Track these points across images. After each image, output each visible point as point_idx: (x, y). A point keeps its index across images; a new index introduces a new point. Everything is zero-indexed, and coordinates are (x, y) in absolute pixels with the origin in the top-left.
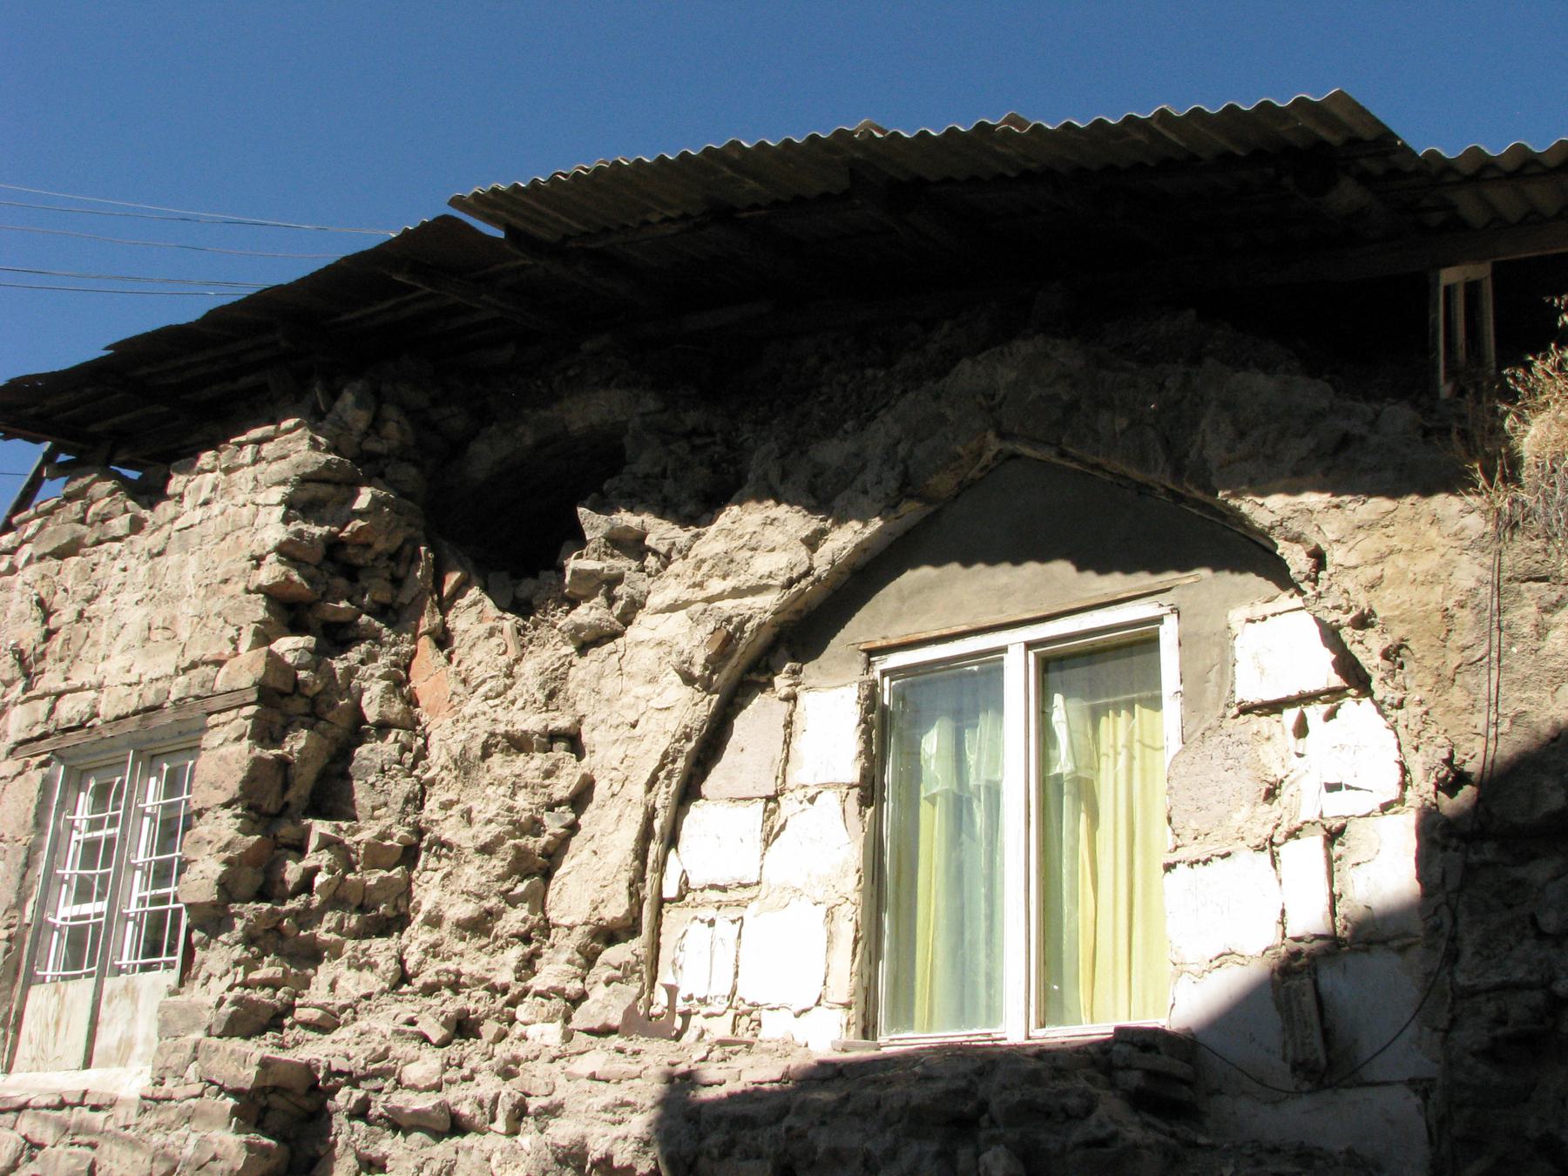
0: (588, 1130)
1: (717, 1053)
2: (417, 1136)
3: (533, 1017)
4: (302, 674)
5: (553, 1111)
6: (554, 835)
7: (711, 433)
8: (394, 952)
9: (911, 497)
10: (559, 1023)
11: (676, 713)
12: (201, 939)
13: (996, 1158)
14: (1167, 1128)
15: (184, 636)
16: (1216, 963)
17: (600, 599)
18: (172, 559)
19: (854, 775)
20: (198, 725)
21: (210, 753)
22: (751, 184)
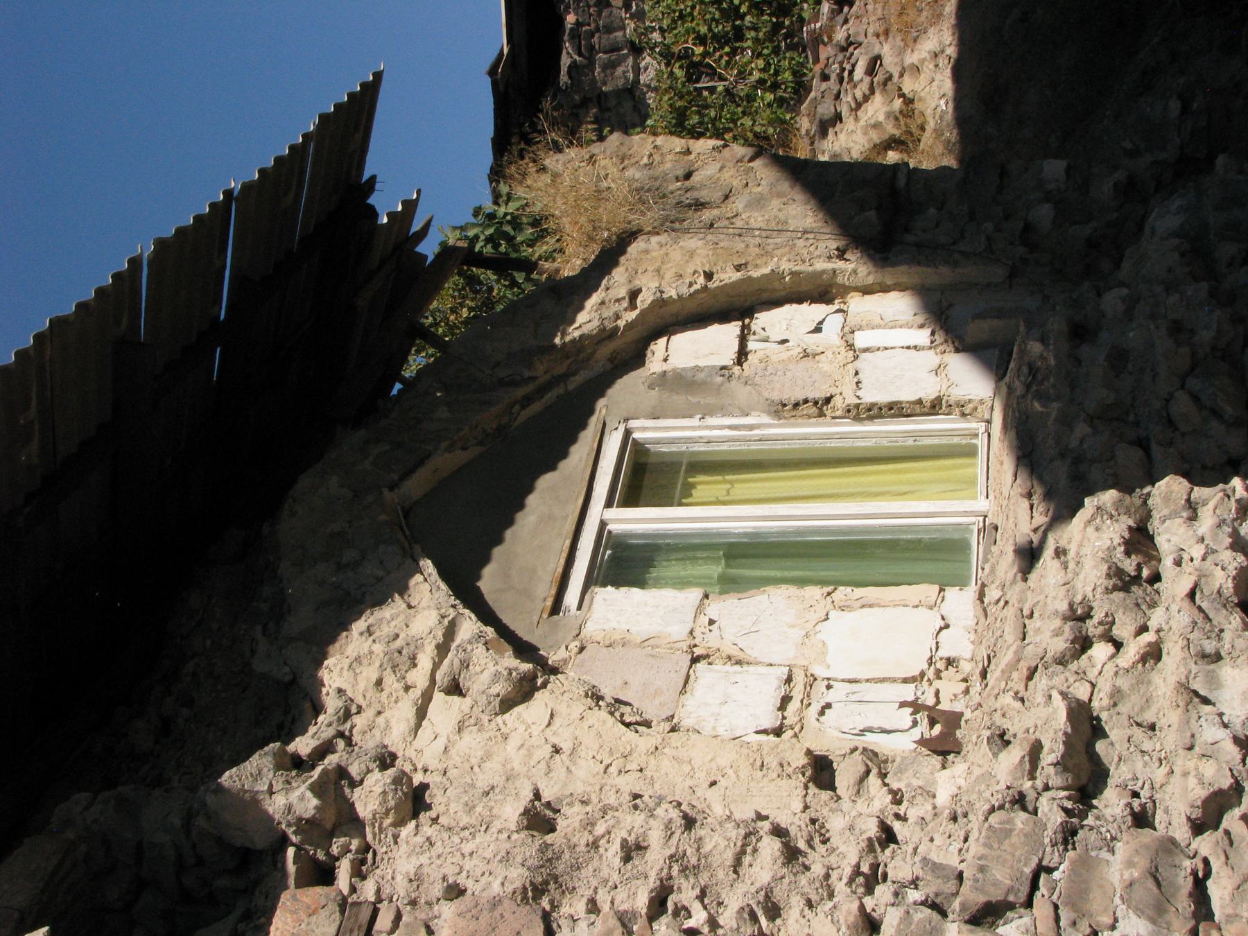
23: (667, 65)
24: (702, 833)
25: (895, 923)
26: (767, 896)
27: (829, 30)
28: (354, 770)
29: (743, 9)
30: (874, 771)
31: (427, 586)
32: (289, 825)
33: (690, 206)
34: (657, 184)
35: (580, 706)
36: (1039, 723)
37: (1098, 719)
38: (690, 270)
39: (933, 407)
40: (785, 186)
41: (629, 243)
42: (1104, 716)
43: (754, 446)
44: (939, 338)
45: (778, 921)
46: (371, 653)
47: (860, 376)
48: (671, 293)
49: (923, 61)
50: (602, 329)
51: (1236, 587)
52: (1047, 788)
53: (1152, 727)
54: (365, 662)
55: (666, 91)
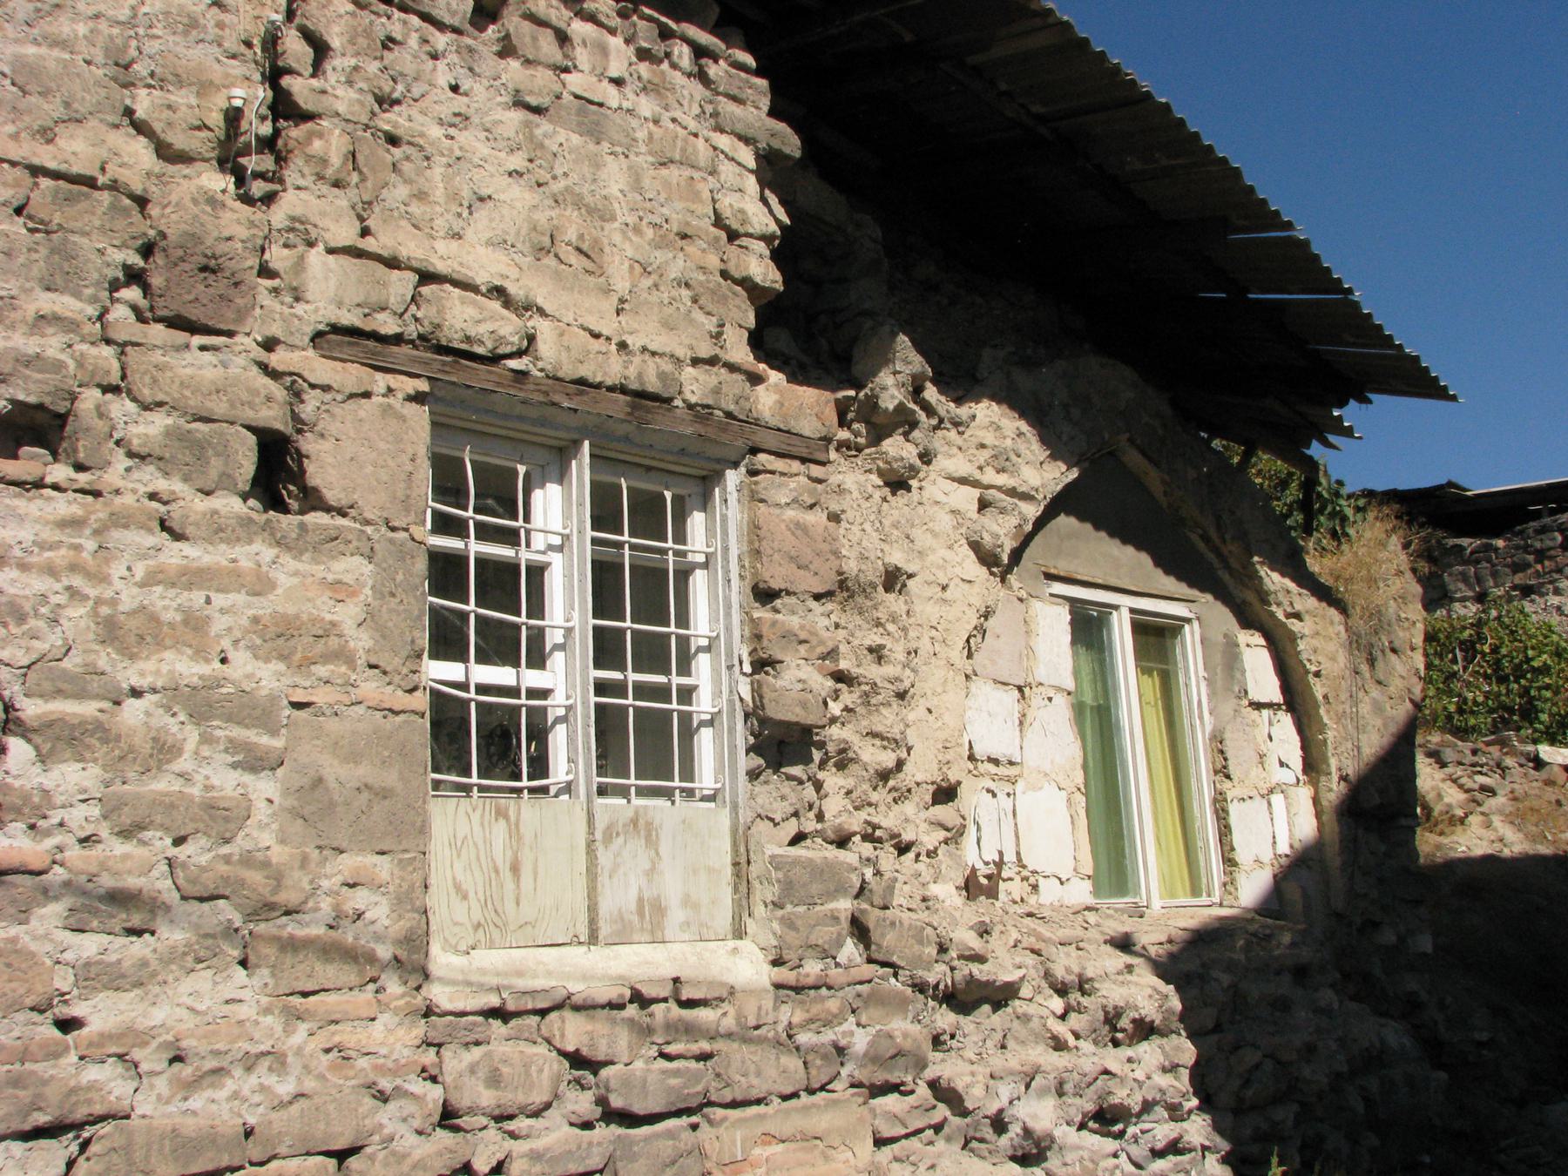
21: (772, 510)
23: (1472, 624)
24: (895, 706)
25: (848, 860)
26: (852, 759)
27: (1513, 752)
28: (916, 434)
29: (1523, 682)
30: (949, 835)
31: (1058, 475)
32: (872, 390)
33: (1371, 654)
34: (1386, 627)
35: (979, 603)
36: (1000, 960)
37: (1006, 1005)
38: (1320, 659)
39: (1230, 860)
40: (1393, 729)
41: (1337, 609)
42: (1009, 1010)
43: (1186, 722)
44: (1284, 861)
45: (834, 770)
46: (1005, 438)
47: (1249, 801)
48: (1301, 646)
49: (1495, 830)
50: (1267, 593)
51: (1115, 1106)
52: (952, 969)
53: (1003, 1047)
54: (998, 434)
55: (1451, 625)
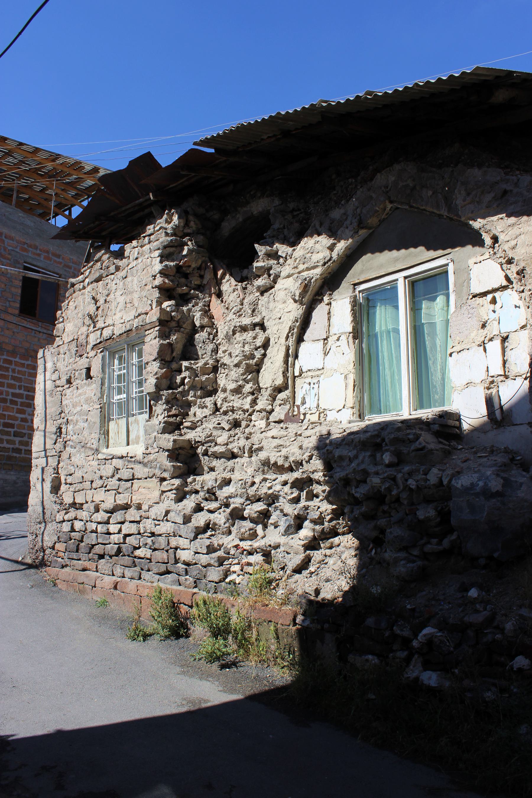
0: (270, 454)
1: (310, 427)
2: (222, 459)
3: (257, 419)
4: (173, 314)
5: (260, 449)
6: (258, 358)
7: (299, 210)
8: (213, 402)
9: (362, 228)
10: (265, 420)
11: (292, 313)
12: (153, 403)
13: (386, 456)
14: (447, 443)
15: (136, 305)
16: (466, 386)
17: (266, 276)
18: (129, 279)
19: (351, 330)
20: (143, 335)
22: (291, 123)
